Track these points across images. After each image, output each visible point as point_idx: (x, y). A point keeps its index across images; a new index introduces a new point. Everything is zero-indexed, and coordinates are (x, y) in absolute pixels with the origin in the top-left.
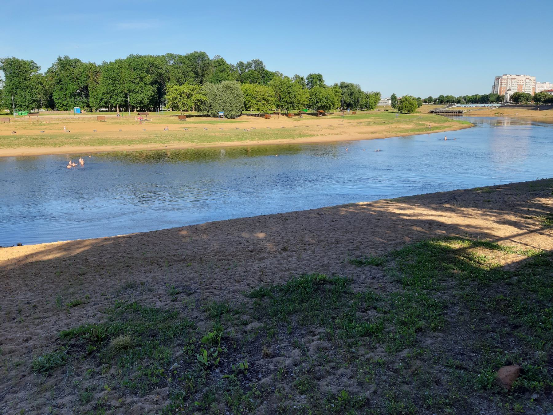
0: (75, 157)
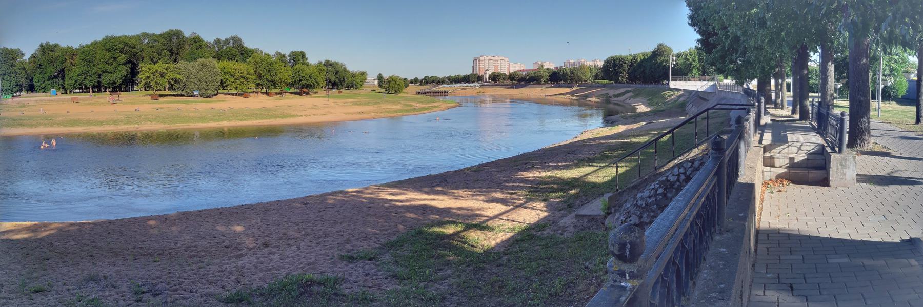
0: (48, 138)
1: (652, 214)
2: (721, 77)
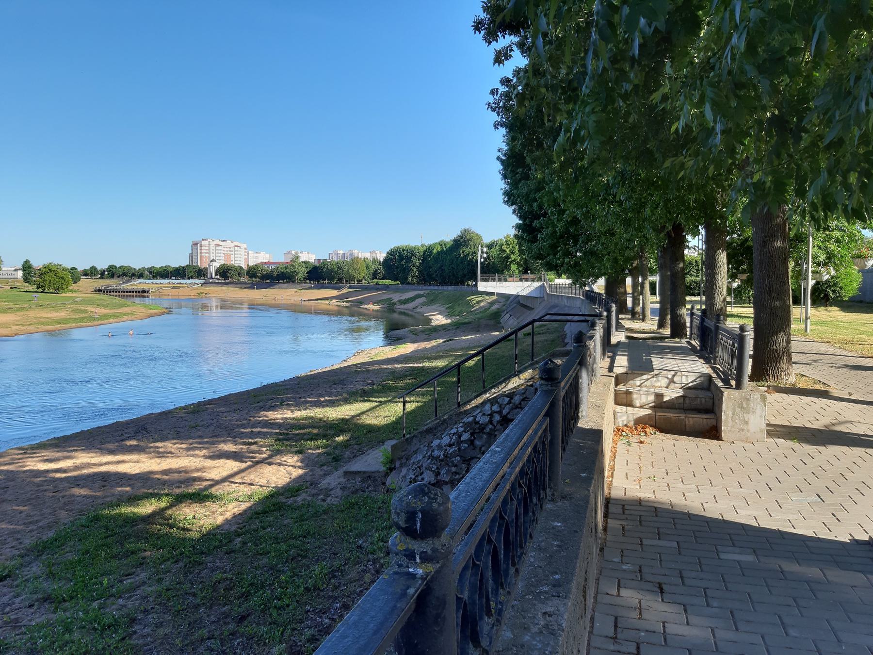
1: (454, 469)
2: (551, 275)
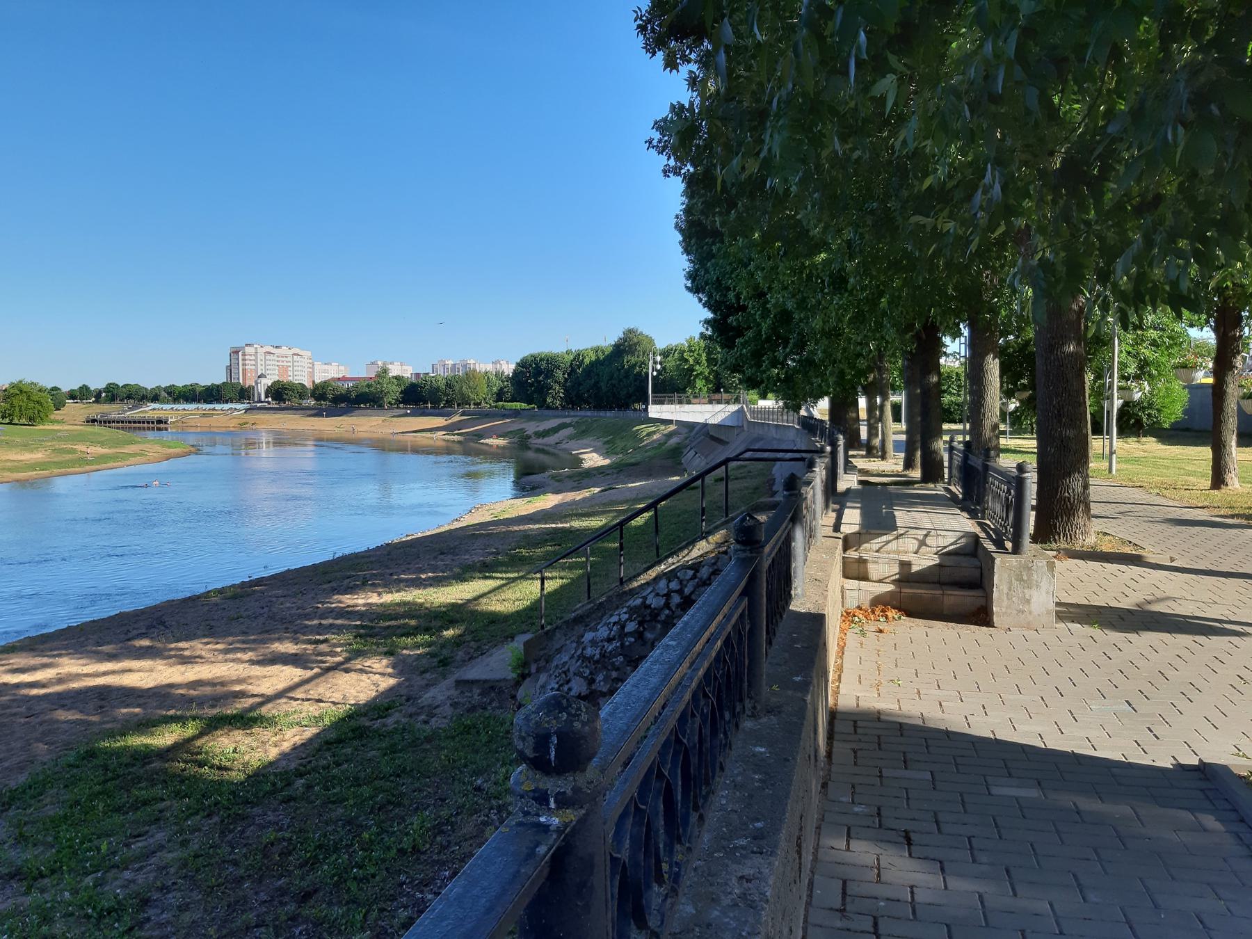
1: (614, 674)
2: (753, 395)
